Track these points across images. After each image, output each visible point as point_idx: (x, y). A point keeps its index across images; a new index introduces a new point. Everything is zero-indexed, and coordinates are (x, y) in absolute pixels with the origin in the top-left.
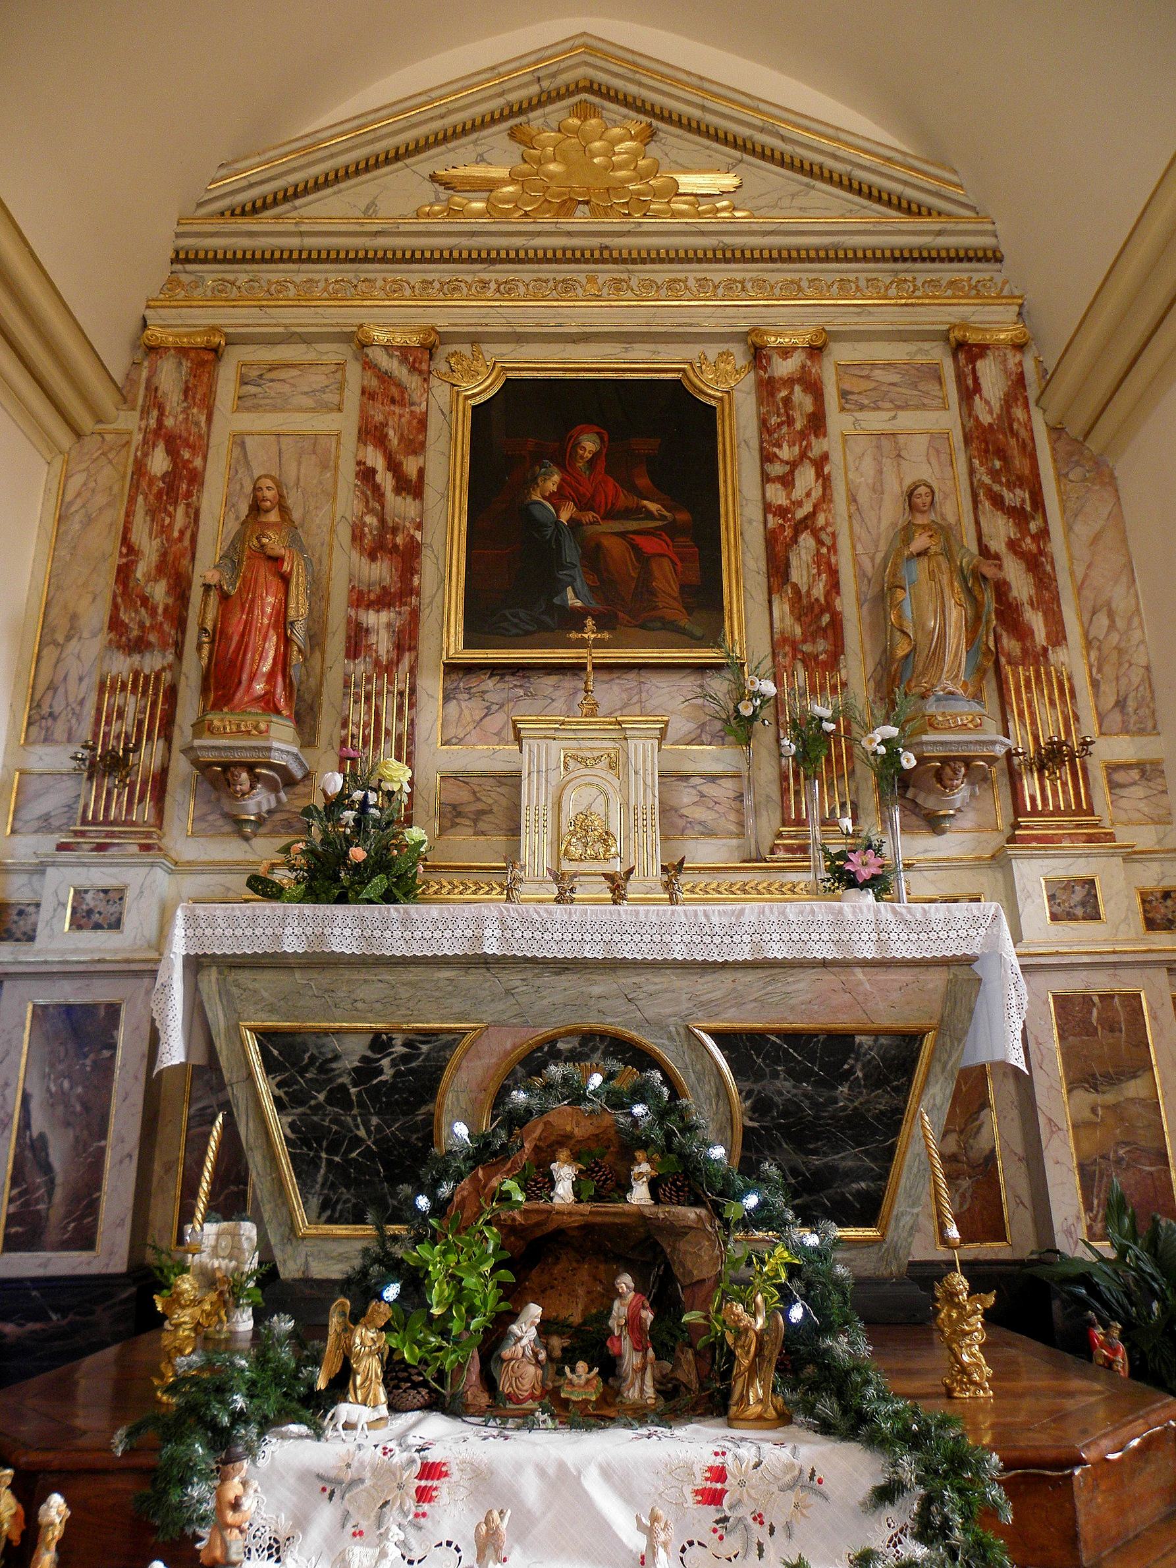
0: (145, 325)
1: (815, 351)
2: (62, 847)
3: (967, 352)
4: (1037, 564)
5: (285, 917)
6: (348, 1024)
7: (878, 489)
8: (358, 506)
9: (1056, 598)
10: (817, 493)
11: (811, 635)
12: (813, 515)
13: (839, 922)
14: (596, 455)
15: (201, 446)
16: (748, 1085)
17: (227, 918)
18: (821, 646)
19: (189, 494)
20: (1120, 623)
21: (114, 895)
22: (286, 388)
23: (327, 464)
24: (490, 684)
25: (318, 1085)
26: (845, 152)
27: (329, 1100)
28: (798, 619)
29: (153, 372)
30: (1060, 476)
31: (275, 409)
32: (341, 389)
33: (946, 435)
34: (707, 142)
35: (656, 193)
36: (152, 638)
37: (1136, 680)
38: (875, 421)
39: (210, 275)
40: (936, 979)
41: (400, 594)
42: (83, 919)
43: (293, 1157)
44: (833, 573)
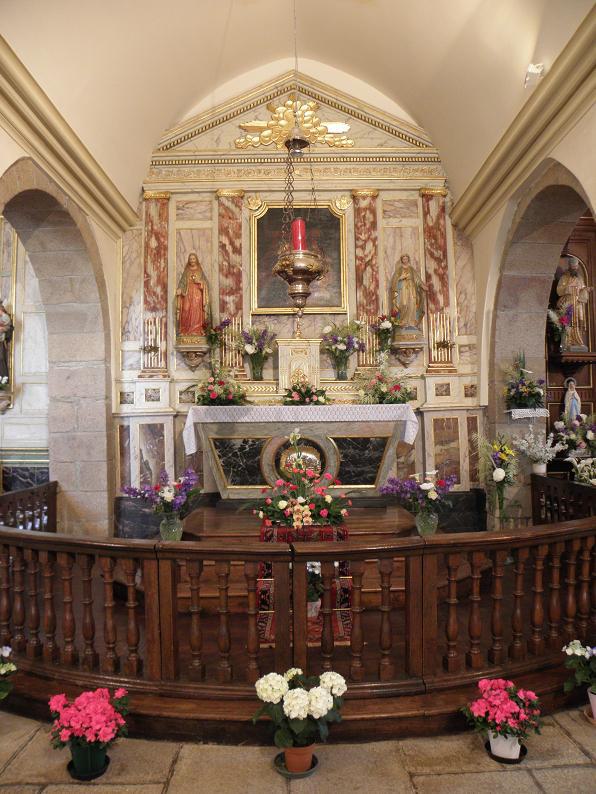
0: (143, 191)
1: (374, 197)
2: (140, 377)
3: (427, 197)
4: (443, 278)
7: (394, 248)
8: (221, 259)
10: (373, 252)
11: (369, 303)
15: (166, 237)
18: (372, 307)
19: (165, 255)
21: (156, 391)
22: (192, 211)
23: (209, 240)
24: (266, 319)
28: (365, 297)
29: (148, 208)
31: (189, 219)
32: (211, 211)
33: (417, 228)
35: (321, 133)
36: (158, 306)
38: (394, 222)
39: (164, 170)
41: (236, 290)
42: (149, 398)
44: (377, 281)
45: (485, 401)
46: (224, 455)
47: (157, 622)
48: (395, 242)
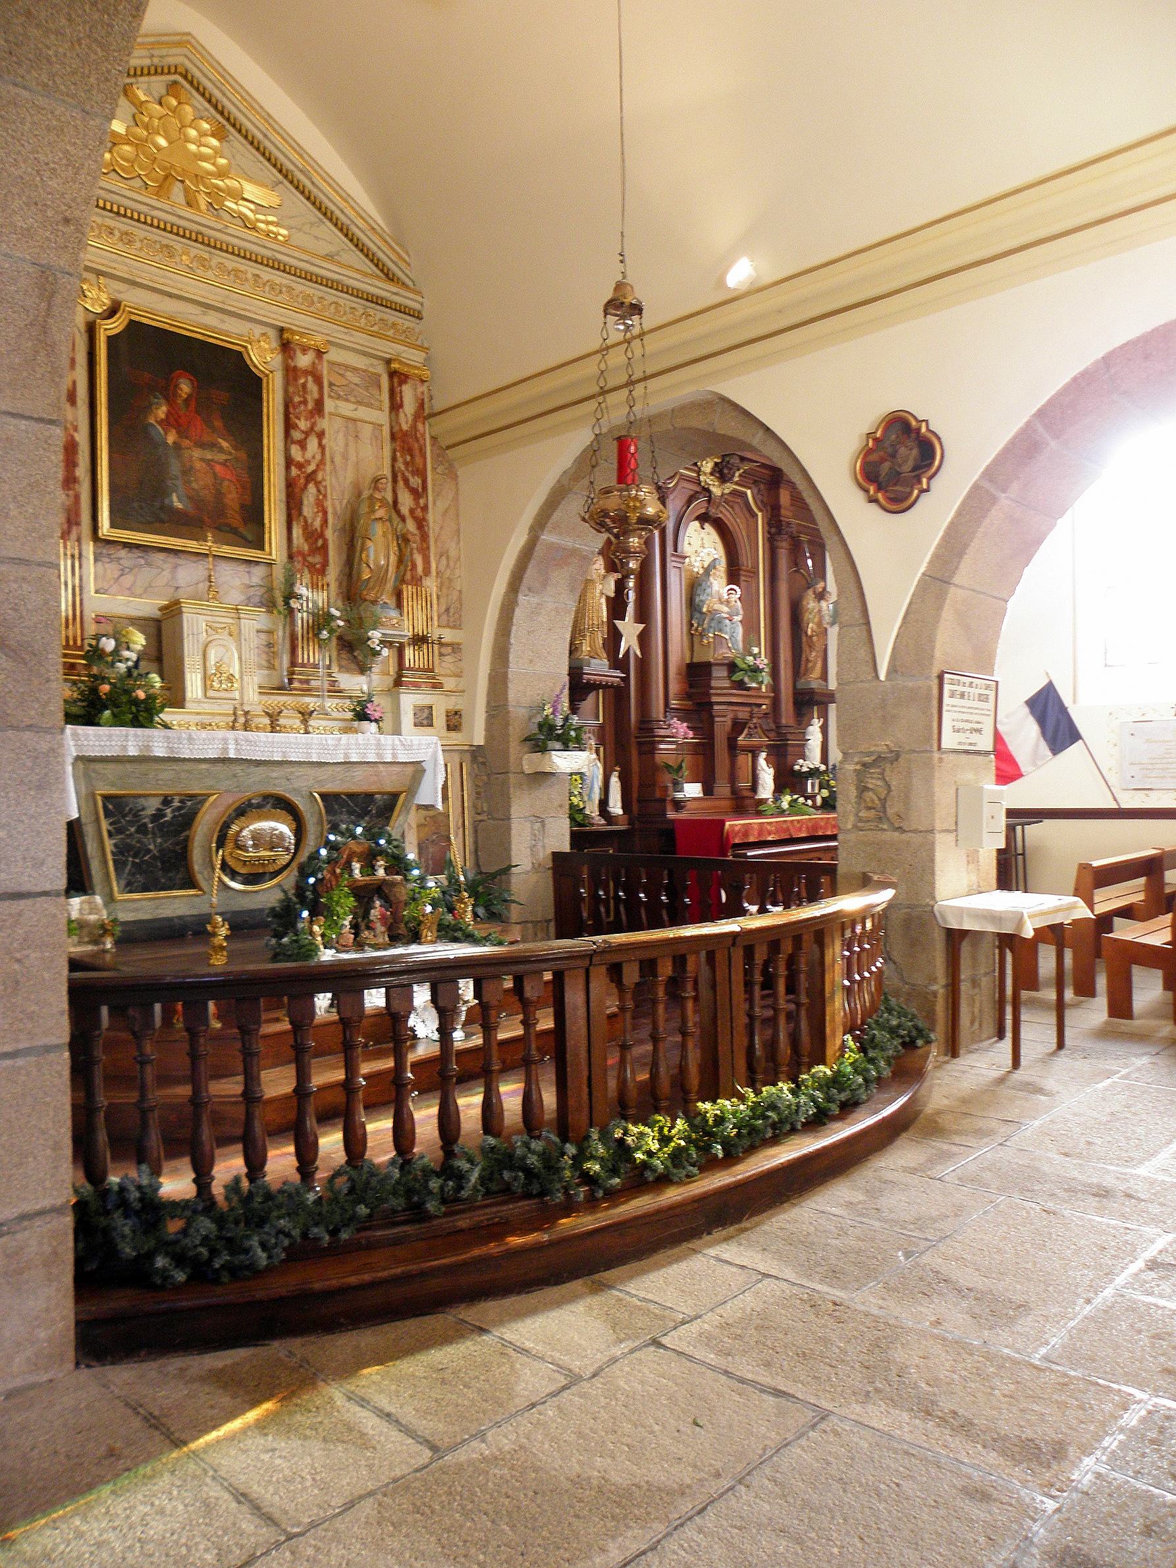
3: (397, 377)
5: (127, 736)
6: (151, 793)
9: (428, 548)
10: (318, 457)
12: (314, 472)
13: (379, 745)
14: (190, 396)
16: (330, 818)
17: (95, 735)
18: (317, 559)
20: (452, 564)
24: (123, 553)
25: (131, 823)
26: (349, 211)
27: (137, 832)
30: (434, 469)
34: (262, 159)
37: (455, 598)
40: (410, 770)
43: (115, 861)
44: (325, 513)
45: (479, 739)
46: (120, 831)
47: (585, 1073)
48: (347, 445)
